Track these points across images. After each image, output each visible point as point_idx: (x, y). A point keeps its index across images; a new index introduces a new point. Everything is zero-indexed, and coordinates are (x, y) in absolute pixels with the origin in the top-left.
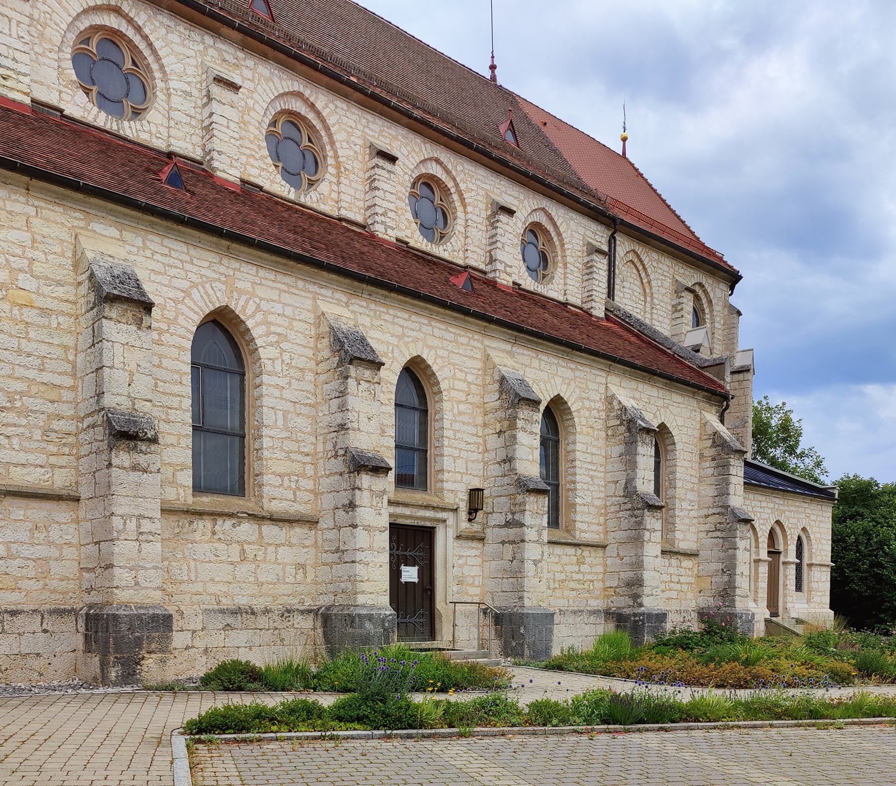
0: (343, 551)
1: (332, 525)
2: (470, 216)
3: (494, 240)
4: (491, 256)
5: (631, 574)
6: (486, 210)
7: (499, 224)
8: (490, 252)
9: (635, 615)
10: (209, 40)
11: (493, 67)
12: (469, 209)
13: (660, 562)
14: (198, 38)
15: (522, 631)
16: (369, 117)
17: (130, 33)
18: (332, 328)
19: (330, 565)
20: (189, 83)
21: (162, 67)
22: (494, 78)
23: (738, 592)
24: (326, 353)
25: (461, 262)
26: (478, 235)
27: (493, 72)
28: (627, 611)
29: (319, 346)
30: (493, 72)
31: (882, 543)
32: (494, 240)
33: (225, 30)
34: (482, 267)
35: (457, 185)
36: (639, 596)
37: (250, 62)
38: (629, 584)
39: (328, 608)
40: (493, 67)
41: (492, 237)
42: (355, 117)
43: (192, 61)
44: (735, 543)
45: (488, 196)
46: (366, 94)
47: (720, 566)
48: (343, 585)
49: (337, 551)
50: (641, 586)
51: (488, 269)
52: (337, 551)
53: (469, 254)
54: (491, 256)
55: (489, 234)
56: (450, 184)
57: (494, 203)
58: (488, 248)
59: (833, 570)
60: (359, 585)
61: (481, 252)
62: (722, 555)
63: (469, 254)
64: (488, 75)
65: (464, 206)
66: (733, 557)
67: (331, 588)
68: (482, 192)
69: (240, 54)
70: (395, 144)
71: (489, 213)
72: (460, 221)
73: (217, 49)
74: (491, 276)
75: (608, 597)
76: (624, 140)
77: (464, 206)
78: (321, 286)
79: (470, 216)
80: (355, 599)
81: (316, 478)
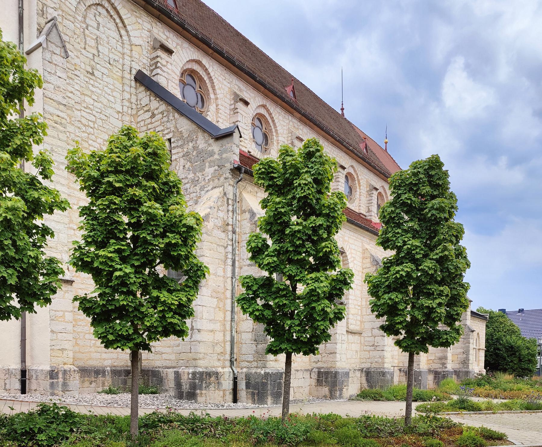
0: (377, 346)
1: (370, 335)
2: (362, 191)
3: (371, 202)
4: (369, 209)
5: (441, 354)
6: (367, 188)
7: (373, 195)
8: (368, 207)
9: (444, 372)
10: (290, 118)
11: (342, 109)
12: (362, 187)
13: (345, 338)
14: (287, 117)
15: (420, 378)
16: (334, 148)
17: (267, 116)
18: (371, 255)
19: (369, 351)
20: (284, 138)
21: (276, 131)
22: (343, 114)
23: (470, 362)
24: (369, 265)
25: (357, 211)
26: (364, 199)
27: (342, 111)
28: (440, 370)
29: (364, 262)
30: (342, 111)
31: (498, 340)
32: (371, 202)
33: (296, 114)
34: (365, 213)
35: (358, 177)
36: (445, 364)
37: (301, 127)
38: (440, 359)
39: (368, 369)
40: (342, 109)
41: (370, 200)
42: (330, 149)
43: (285, 128)
44: (469, 341)
45: (367, 181)
46: (336, 140)
47: (462, 350)
48: (376, 360)
49: (373, 345)
50: (446, 359)
51: (367, 214)
52: (373, 345)
53: (361, 208)
54: (369, 209)
55: (368, 199)
56: (355, 177)
57: (370, 185)
58: (368, 205)
59: (486, 351)
60: (385, 360)
61: (365, 207)
62: (463, 346)
63: (361, 208)
64: (340, 112)
65: (360, 186)
66: (469, 347)
67: (370, 361)
68: (365, 180)
69: (299, 124)
70: (341, 160)
71: (368, 189)
72: (358, 193)
73: (293, 122)
74: (368, 218)
75: (429, 364)
76: (386, 143)
77: (360, 186)
78: (364, 237)
79: (362, 191)
80: (383, 365)
81: (362, 316)
